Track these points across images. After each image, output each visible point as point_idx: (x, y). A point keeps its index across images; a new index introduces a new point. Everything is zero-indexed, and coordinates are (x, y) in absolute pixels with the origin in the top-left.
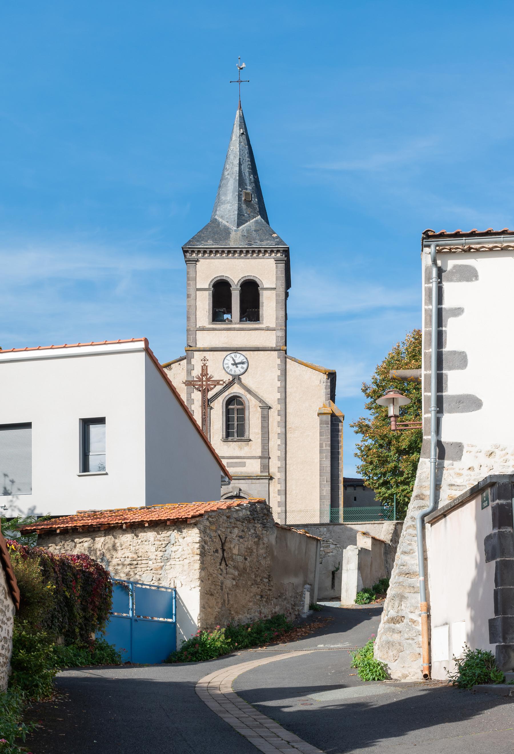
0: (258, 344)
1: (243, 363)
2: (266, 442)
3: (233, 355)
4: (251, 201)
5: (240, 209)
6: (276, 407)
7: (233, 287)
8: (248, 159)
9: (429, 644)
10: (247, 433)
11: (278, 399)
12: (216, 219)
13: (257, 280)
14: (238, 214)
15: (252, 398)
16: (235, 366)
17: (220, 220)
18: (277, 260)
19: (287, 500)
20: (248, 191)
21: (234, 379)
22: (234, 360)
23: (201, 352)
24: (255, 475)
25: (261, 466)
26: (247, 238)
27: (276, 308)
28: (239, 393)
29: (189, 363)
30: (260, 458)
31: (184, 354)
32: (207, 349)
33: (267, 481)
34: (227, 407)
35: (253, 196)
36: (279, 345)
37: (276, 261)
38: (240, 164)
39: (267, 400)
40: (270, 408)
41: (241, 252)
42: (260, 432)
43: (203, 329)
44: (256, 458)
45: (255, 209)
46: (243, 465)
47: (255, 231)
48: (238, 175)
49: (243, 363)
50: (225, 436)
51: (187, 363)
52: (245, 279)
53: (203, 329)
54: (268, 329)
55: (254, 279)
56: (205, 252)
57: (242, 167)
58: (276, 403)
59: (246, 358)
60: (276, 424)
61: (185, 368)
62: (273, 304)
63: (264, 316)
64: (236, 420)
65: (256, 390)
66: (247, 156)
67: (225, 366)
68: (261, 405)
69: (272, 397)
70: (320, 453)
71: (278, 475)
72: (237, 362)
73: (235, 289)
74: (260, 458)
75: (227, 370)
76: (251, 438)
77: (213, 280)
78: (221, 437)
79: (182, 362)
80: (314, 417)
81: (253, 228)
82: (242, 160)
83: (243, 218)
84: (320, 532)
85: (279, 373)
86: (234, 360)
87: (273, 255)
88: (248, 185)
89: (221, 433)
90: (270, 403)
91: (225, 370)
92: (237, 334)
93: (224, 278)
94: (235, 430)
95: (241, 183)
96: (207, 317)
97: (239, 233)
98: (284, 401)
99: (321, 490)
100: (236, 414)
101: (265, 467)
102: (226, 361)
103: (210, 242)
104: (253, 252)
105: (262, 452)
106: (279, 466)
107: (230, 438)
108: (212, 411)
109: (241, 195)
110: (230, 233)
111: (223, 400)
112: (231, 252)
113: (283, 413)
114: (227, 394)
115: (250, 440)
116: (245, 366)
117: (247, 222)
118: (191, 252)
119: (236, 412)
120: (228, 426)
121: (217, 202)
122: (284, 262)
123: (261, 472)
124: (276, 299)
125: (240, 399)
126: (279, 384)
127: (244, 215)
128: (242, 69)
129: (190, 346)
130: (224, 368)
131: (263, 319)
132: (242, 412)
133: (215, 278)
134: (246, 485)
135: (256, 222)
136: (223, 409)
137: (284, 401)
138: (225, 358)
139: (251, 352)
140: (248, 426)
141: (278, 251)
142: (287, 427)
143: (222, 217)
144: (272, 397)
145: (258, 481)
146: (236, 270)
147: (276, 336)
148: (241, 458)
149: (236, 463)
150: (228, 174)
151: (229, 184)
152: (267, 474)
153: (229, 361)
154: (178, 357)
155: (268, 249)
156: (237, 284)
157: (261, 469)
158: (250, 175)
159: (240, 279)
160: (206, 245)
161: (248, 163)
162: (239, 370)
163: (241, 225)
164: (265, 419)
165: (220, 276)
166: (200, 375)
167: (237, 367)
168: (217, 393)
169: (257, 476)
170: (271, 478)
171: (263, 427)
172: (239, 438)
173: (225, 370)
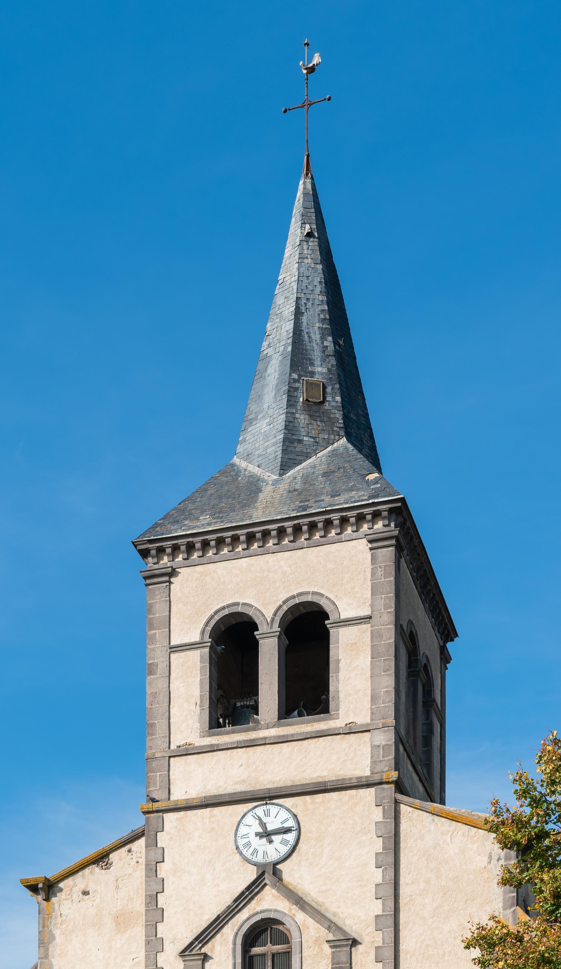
0: (325, 773)
1: (287, 831)
3: (260, 811)
5: (290, 427)
6: (372, 938)
7: (263, 628)
8: (321, 298)
11: (377, 916)
12: (233, 465)
13: (323, 602)
15: (310, 922)
16: (264, 840)
17: (243, 464)
18: (375, 541)
20: (317, 378)
21: (263, 873)
22: (263, 824)
23: (182, 813)
26: (299, 494)
27: (372, 669)
28: (276, 911)
29: (153, 844)
31: (139, 822)
32: (195, 803)
35: (329, 390)
36: (378, 768)
38: (298, 313)
39: (348, 922)
40: (355, 943)
41: (281, 532)
43: (187, 751)
45: (332, 421)
47: (325, 474)
48: (290, 341)
49: (287, 831)
51: (147, 846)
52: (291, 603)
53: (187, 751)
54: (351, 730)
55: (315, 599)
56: (190, 548)
57: (304, 319)
58: (372, 928)
59: (295, 816)
61: (143, 861)
62: (364, 661)
63: (341, 695)
65: (320, 900)
66: (318, 289)
67: (241, 842)
68: (331, 937)
69: (360, 913)
72: (270, 827)
73: (267, 635)
75: (244, 852)
77: (212, 617)
82: (303, 301)
83: (299, 447)
85: (378, 845)
86: (263, 824)
88: (318, 362)
90: (353, 928)
91: (241, 854)
93: (240, 609)
95: (299, 357)
96: (196, 718)
97: (283, 487)
98: (391, 921)
102: (243, 830)
103: (205, 518)
104: (313, 527)
110: (259, 490)
111: (236, 934)
113: (389, 953)
116: (291, 837)
117: (308, 456)
118: (161, 551)
122: (393, 542)
124: (372, 646)
125: (281, 928)
126: (378, 876)
127: (300, 441)
128: (311, 70)
129: (154, 800)
130: (237, 848)
133: (216, 613)
135: (334, 453)
136: (234, 957)
139: (308, 798)
141: (376, 515)
144: (360, 913)
146: (263, 584)
150: (269, 346)
151: (270, 370)
153: (251, 826)
154: (125, 833)
155: (349, 514)
156: (273, 620)
158: (323, 339)
159: (280, 607)
160: (193, 528)
161: (320, 308)
163: (291, 467)
165: (228, 606)
167: (271, 842)
168: (218, 917)
173: (241, 854)
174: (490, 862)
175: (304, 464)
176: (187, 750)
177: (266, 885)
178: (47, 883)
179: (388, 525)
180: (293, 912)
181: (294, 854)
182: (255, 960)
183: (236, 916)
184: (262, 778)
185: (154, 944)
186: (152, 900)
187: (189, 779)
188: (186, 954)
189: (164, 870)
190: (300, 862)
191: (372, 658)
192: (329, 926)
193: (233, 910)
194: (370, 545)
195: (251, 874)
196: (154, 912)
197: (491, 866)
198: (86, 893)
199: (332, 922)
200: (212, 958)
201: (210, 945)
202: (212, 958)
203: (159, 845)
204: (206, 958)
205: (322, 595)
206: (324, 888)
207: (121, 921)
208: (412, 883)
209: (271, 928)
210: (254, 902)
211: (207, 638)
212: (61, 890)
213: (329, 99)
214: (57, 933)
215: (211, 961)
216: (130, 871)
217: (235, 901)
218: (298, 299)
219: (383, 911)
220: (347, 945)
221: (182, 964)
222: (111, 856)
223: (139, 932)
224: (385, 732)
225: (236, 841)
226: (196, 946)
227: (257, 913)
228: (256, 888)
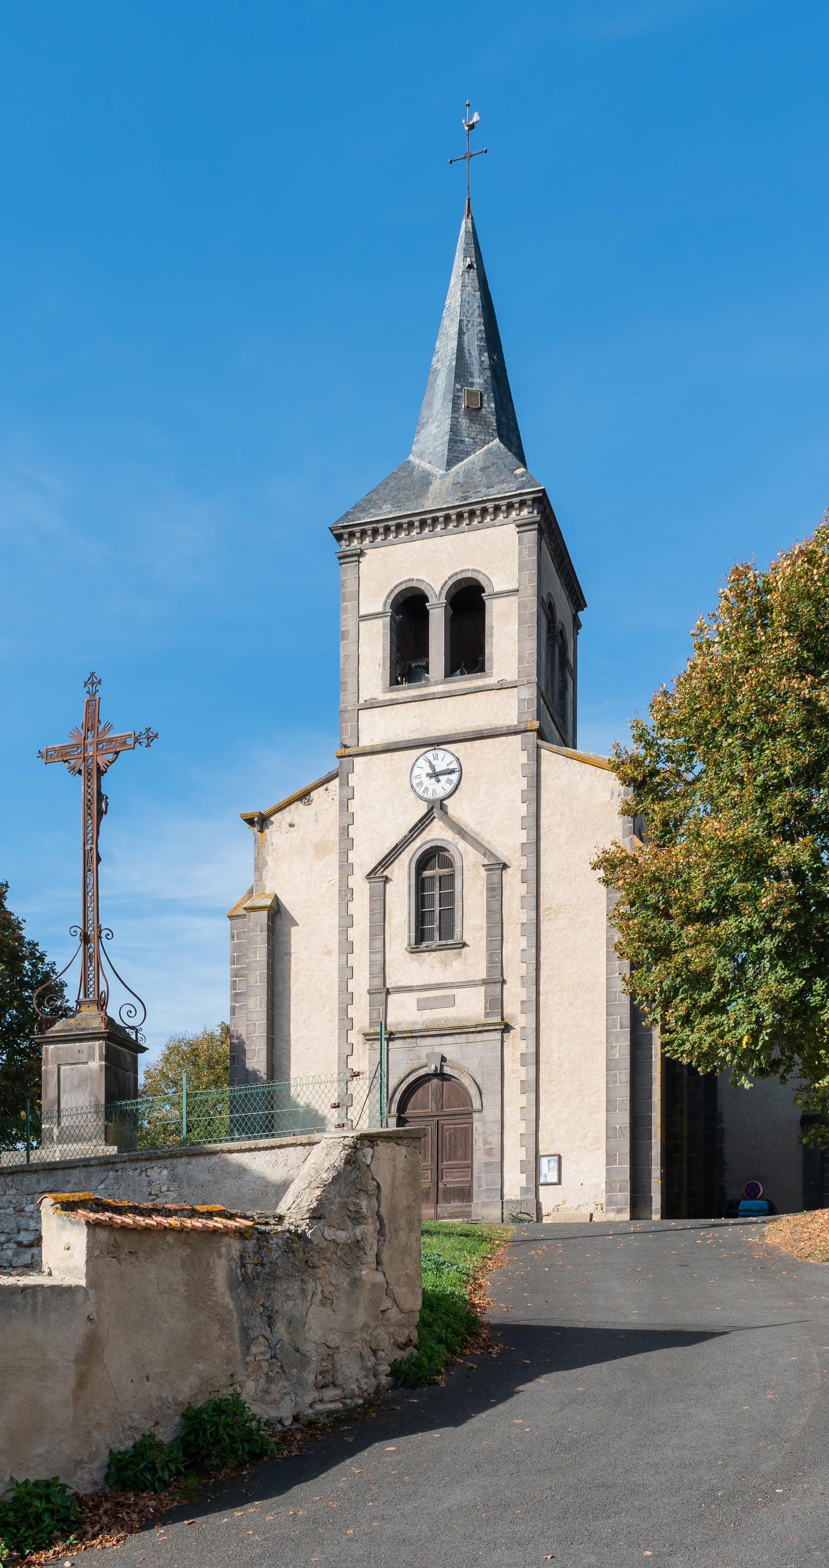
0: (482, 723)
1: (452, 772)
3: (430, 755)
4: (480, 408)
5: (454, 430)
6: (518, 863)
7: (432, 600)
8: (479, 320)
10: (457, 929)
11: (523, 844)
12: (409, 462)
14: (450, 440)
16: (433, 779)
19: (541, 1076)
20: (476, 388)
21: (432, 808)
22: (432, 767)
24: (473, 1023)
25: (486, 1000)
27: (519, 634)
28: (443, 840)
29: (345, 784)
30: (485, 982)
31: (333, 765)
33: (498, 1035)
35: (485, 398)
36: (524, 719)
37: (518, 526)
38: (461, 333)
39: (499, 849)
40: (505, 866)
42: (485, 924)
43: (372, 705)
44: (476, 985)
45: (487, 425)
46: (451, 1002)
48: (455, 356)
49: (452, 772)
50: (413, 941)
51: (340, 785)
53: (372, 705)
54: (502, 687)
57: (466, 338)
58: (518, 854)
60: (517, 903)
61: (337, 798)
62: (513, 627)
63: (495, 657)
64: (437, 902)
65: (477, 830)
66: (477, 313)
68: (486, 862)
69: (509, 842)
70: (607, 961)
71: (521, 1021)
72: (438, 769)
73: (435, 606)
75: (417, 790)
76: (466, 939)
77: (392, 591)
78: (405, 945)
81: (480, 464)
82: (465, 323)
84: (150, 1183)
85: (523, 784)
86: (432, 767)
87: (514, 513)
89: (407, 934)
91: (415, 791)
92: (445, 706)
95: (461, 371)
96: (380, 677)
97: (449, 480)
99: (609, 1048)
100: (438, 889)
101: (496, 1004)
102: (416, 771)
103: (387, 507)
104: (472, 514)
106: (524, 998)
108: (388, 886)
109: (459, 397)
110: (430, 483)
111: (411, 859)
112: (427, 522)
113: (532, 875)
115: (464, 945)
116: (454, 777)
117: (468, 454)
118: (352, 535)
119: (437, 884)
120: (421, 918)
121: (413, 426)
122: (536, 526)
123: (487, 1015)
124: (519, 615)
125: (446, 854)
127: (462, 442)
128: (472, 127)
129: (346, 746)
130: (412, 787)
131: (492, 665)
132: (448, 881)
133: (396, 587)
134: (455, 1048)
135: (489, 452)
136: (409, 879)
137: (535, 847)
138: (414, 765)
139: (468, 744)
140: (460, 913)
141: (523, 504)
142: (542, 908)
143: (421, 455)
144: (509, 842)
145: (479, 1037)
147: (519, 700)
148: (446, 988)
149: (436, 998)
152: (498, 1019)
154: (323, 775)
156: (440, 593)
157: (486, 1008)
158: (480, 354)
159: (446, 582)
161: (479, 328)
163: (455, 464)
164: (495, 891)
166: (80, 728)
168: (397, 845)
169: (477, 1026)
170: (507, 1028)
171: (490, 912)
172: (444, 942)
173: (415, 791)
174: (612, 798)
175: (465, 461)
176: (372, 703)
177: (434, 818)
179: (532, 512)
182: (426, 881)
184: (431, 727)
185: (346, 868)
186: (344, 831)
187: (374, 728)
189: (354, 806)
194: (517, 530)
195: (423, 809)
196: (346, 841)
197: (613, 801)
201: (390, 869)
204: (387, 880)
205: (480, 572)
206: (480, 820)
207: (320, 849)
210: (425, 832)
211: (388, 609)
212: (272, 823)
213: (486, 151)
214: (269, 859)
217: (410, 831)
218: (461, 321)
220: (498, 869)
221: (368, 885)
222: (312, 794)
223: (334, 858)
224: (529, 687)
225: (411, 781)
227: (428, 842)
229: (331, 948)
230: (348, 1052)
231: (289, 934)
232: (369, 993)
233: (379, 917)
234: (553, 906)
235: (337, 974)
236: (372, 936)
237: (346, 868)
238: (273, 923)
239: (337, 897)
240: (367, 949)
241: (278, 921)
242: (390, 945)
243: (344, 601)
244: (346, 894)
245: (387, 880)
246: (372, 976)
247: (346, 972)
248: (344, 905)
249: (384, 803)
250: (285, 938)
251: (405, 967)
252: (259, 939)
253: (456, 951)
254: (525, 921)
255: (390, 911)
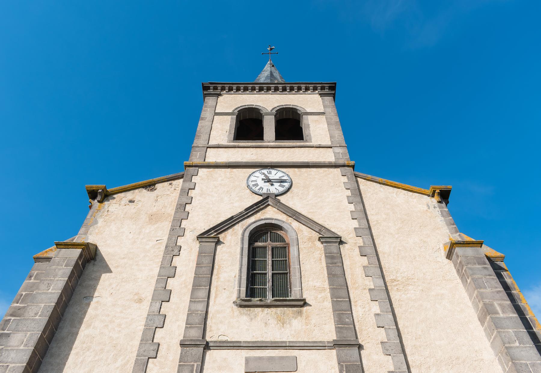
2: (345, 306)
9: (164, 321)
11: (355, 229)
30: (336, 345)
34: (251, 243)
40: (341, 242)
42: (326, 285)
50: (243, 295)
58: (353, 234)
60: (359, 272)
64: (269, 267)
67: (251, 184)
69: (343, 225)
74: (336, 345)
78: (234, 297)
79: (174, 182)
80: (439, 259)
89: (237, 288)
94: (269, 285)
105: (338, 330)
107: (256, 300)
108: (219, 247)
111: (245, 230)
113: (370, 250)
114: (252, 221)
115: (304, 303)
116: (287, 185)
118: (212, 89)
130: (248, 186)
132: (282, 253)
136: (242, 243)
139: (296, 169)
140: (298, 274)
162: (276, 188)
168: (232, 218)
171: (331, 276)
174: (429, 208)
177: (269, 205)
178: (105, 192)
180: (290, 221)
181: (288, 193)
182: (258, 250)
183: (246, 220)
185: (176, 230)
188: (205, 236)
190: (293, 197)
191: (328, 125)
192: (320, 230)
193: (244, 215)
198: (131, 201)
199: (323, 227)
200: (224, 243)
202: (224, 243)
203: (193, 181)
204: (218, 242)
206: (311, 211)
208: (376, 214)
209: (271, 232)
212: (114, 198)
214: (100, 222)
215: (222, 245)
216: (168, 193)
217: (246, 210)
219: (360, 225)
220: (336, 242)
223: (167, 225)
225: (247, 183)
226: (212, 234)
227: (262, 220)
228: (262, 205)
229: (143, 296)
230: (159, 323)
231: (98, 279)
232: (182, 345)
233: (206, 270)
234: (399, 279)
235: (143, 323)
236: (196, 286)
237: (176, 230)
238: (84, 266)
239: (162, 253)
240: (188, 298)
241: (90, 267)
242: (216, 297)
243: (206, 107)
244: (173, 250)
245: (218, 242)
246: (189, 325)
247: (156, 321)
248: (169, 257)
249: (220, 192)
250: (91, 283)
251: (228, 319)
252: (60, 273)
253: (295, 309)
254: (373, 287)
255: (220, 267)
